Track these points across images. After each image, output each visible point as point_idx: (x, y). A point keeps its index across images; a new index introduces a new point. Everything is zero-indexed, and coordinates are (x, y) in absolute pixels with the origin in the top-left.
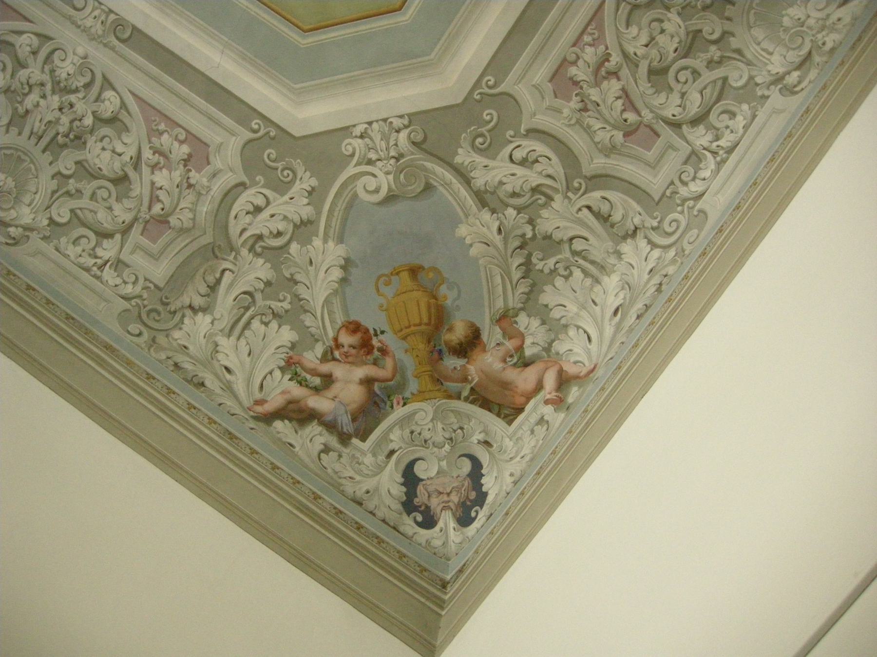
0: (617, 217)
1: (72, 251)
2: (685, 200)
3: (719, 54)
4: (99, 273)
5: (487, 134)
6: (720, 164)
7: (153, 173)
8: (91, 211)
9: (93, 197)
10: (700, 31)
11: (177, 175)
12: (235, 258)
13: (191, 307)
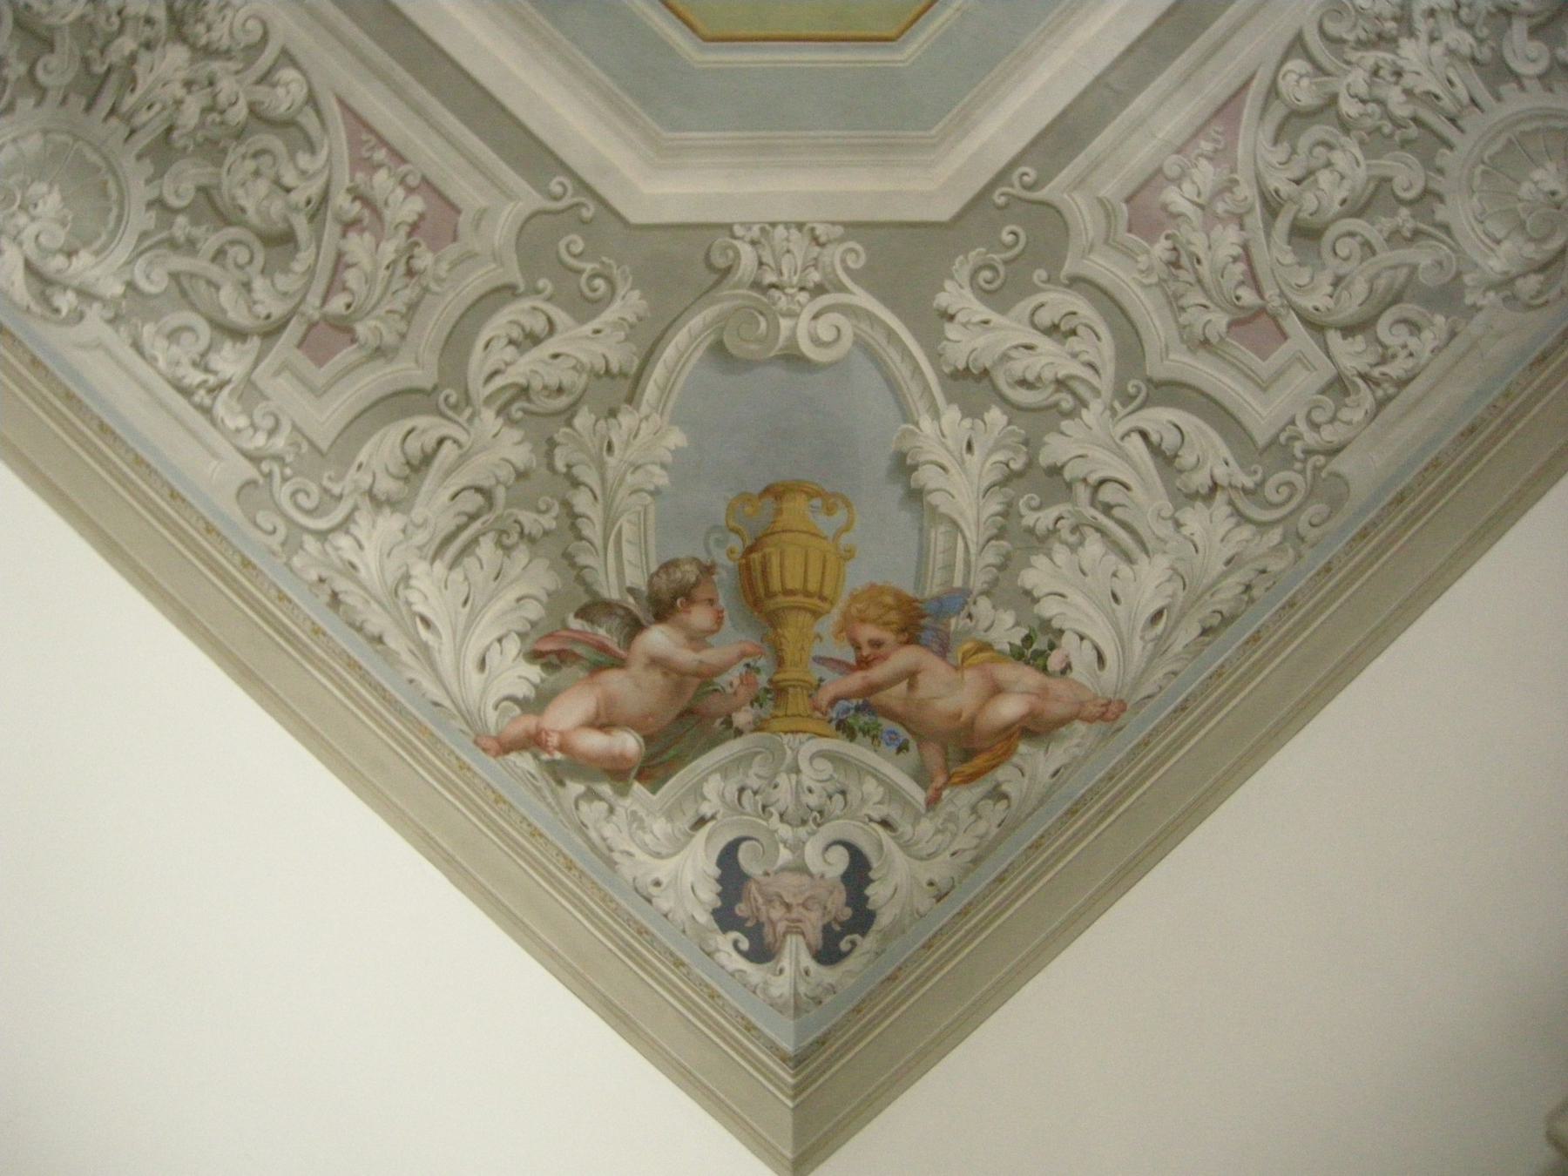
0: (1187, 458)
1: (160, 349)
2: (1308, 452)
3: (1410, 224)
4: (207, 401)
5: (1002, 269)
6: (1381, 404)
7: (344, 235)
8: (210, 283)
9: (219, 255)
10: (1389, 180)
11: (389, 249)
12: (470, 420)
13: (371, 494)
